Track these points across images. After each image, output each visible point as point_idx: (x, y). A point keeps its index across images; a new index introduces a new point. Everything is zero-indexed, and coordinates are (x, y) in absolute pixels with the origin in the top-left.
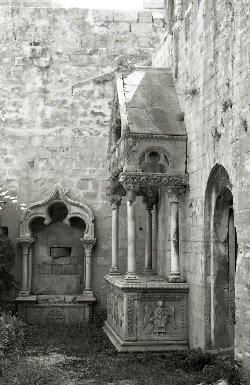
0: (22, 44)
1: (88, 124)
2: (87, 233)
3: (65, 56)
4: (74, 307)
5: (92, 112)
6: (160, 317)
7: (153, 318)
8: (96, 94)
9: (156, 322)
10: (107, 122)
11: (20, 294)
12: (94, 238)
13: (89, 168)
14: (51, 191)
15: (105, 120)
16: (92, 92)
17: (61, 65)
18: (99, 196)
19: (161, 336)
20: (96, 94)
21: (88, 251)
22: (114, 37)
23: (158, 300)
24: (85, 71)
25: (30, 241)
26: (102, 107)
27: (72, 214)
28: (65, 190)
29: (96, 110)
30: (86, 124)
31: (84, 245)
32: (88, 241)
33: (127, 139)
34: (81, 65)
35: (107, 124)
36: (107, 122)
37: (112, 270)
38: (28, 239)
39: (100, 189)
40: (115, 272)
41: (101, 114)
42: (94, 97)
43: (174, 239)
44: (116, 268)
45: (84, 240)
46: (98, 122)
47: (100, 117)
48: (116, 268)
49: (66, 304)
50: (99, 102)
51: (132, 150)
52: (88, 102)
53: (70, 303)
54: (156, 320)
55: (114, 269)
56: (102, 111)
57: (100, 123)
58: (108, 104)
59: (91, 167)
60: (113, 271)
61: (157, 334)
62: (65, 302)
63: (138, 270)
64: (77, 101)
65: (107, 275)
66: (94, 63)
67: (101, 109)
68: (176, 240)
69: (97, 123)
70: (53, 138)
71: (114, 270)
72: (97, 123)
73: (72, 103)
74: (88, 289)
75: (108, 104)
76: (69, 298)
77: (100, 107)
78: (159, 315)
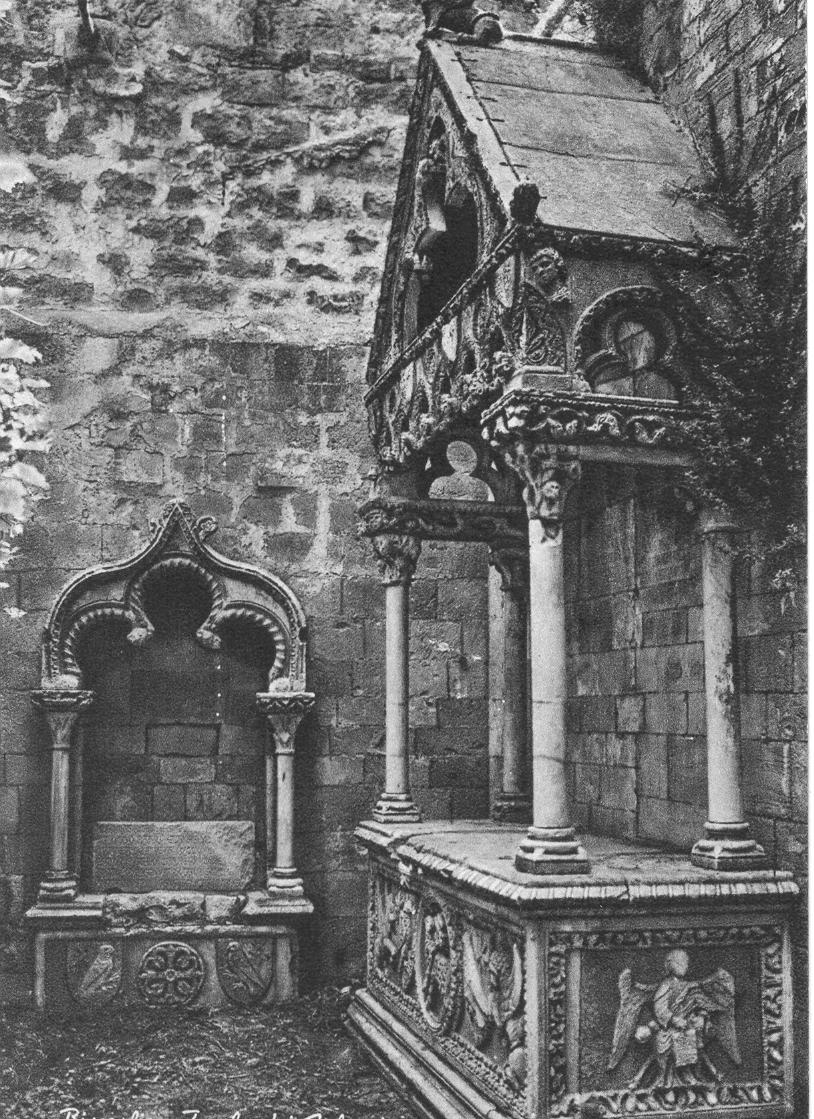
0: (48, 16)
1: (277, 304)
2: (281, 673)
3: (199, 69)
4: (235, 936)
5: (292, 263)
6: (680, 1021)
7: (652, 1023)
8: (306, 202)
9: (663, 1045)
10: (343, 299)
11: (42, 892)
12: (308, 689)
13: (282, 452)
14: (154, 525)
15: (335, 291)
16: (293, 195)
17: (184, 99)
18: (319, 548)
19: (685, 1105)
20: (306, 202)
21: (285, 737)
22: (365, 17)
23: (670, 949)
24: (268, 122)
25: (80, 700)
26: (326, 248)
27: (229, 607)
28: (203, 521)
29: (306, 258)
30: (272, 304)
31: (270, 717)
32: (286, 702)
33: (529, 254)
34: (252, 101)
35: (344, 304)
36: (343, 299)
37: (389, 804)
38: (74, 695)
39: (323, 521)
40: (401, 811)
41: (319, 270)
42: (297, 213)
43: (723, 686)
44: (403, 797)
45: (273, 699)
46: (312, 298)
47: (317, 283)
48: (403, 797)
49: (209, 928)
50: (315, 231)
51: (555, 297)
52: (280, 229)
53: (220, 921)
54: (662, 1033)
55: (397, 800)
56: (324, 260)
57: (319, 300)
58: (347, 239)
59: (290, 446)
60: (390, 808)
61: (670, 1097)
62: (204, 920)
63: (585, 819)
64: (240, 223)
65: (362, 823)
66: (297, 99)
67: (323, 255)
68: (732, 689)
69: (310, 302)
70: (157, 344)
71: (396, 805)
72: (310, 302)
73: (224, 230)
74: (288, 871)
75: (347, 239)
76: (218, 905)
77: (319, 248)
78: (676, 1014)
